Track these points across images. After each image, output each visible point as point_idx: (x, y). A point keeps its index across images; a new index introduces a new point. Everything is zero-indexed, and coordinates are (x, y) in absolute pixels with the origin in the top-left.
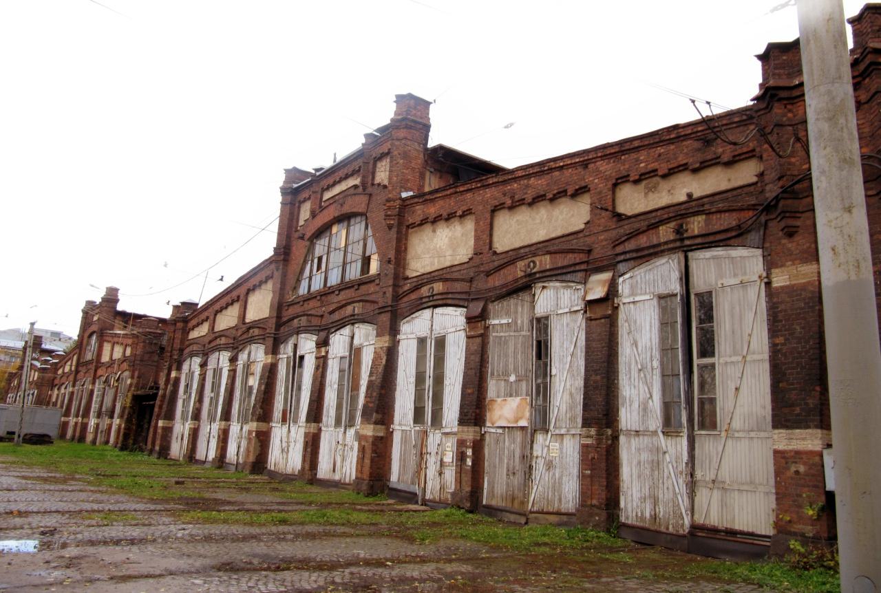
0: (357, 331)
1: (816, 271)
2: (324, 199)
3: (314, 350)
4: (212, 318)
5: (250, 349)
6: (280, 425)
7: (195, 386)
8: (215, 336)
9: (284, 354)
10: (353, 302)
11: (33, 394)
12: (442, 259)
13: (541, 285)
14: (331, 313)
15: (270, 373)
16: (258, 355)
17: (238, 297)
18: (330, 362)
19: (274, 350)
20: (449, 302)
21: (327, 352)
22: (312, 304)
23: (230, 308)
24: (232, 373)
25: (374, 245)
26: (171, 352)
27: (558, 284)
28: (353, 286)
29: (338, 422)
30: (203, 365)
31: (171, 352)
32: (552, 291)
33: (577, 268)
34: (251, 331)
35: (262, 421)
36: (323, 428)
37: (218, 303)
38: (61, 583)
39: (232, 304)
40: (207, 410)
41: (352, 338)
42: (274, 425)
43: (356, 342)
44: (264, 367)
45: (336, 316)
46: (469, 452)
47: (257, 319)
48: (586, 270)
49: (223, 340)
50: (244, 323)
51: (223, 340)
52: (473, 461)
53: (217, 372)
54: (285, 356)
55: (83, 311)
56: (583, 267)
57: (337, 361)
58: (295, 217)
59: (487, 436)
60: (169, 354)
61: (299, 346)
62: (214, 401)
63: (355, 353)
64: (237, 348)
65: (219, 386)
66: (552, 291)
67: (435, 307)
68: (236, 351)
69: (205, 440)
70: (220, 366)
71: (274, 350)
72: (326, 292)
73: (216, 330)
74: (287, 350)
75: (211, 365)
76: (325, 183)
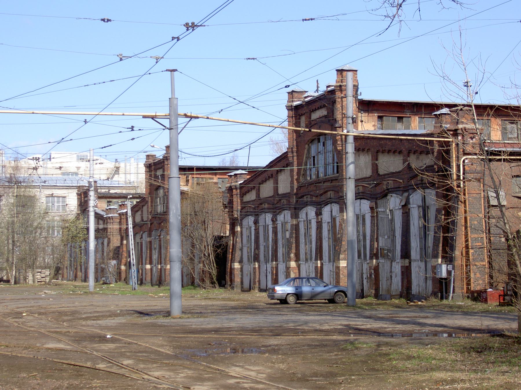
0: (333, 208)
1: (330, 210)
3: (315, 217)
5: (307, 210)
6: (304, 263)
9: (302, 218)
10: (329, 191)
12: (128, 176)
13: (390, 194)
15: (296, 228)
16: (285, 217)
17: (272, 175)
18: (323, 225)
19: (295, 216)
22: (312, 188)
23: (268, 182)
24: (275, 229)
28: (329, 181)
29: (330, 261)
30: (256, 222)
32: (159, 212)
36: (324, 264)
37: (260, 177)
38: (411, 335)
40: (247, 256)
41: (332, 212)
42: (301, 263)
43: (333, 214)
44: (292, 225)
47: (285, 192)
49: (266, 206)
50: (278, 195)
52: (375, 276)
53: (266, 227)
54: (302, 220)
55: (144, 165)
57: (326, 224)
59: (380, 264)
61: (308, 214)
62: (266, 247)
65: (268, 240)
66: (159, 212)
67: (361, 199)
69: (265, 275)
70: (267, 224)
71: (295, 216)
72: (318, 182)
74: (302, 215)
75: (261, 223)
76: (313, 107)
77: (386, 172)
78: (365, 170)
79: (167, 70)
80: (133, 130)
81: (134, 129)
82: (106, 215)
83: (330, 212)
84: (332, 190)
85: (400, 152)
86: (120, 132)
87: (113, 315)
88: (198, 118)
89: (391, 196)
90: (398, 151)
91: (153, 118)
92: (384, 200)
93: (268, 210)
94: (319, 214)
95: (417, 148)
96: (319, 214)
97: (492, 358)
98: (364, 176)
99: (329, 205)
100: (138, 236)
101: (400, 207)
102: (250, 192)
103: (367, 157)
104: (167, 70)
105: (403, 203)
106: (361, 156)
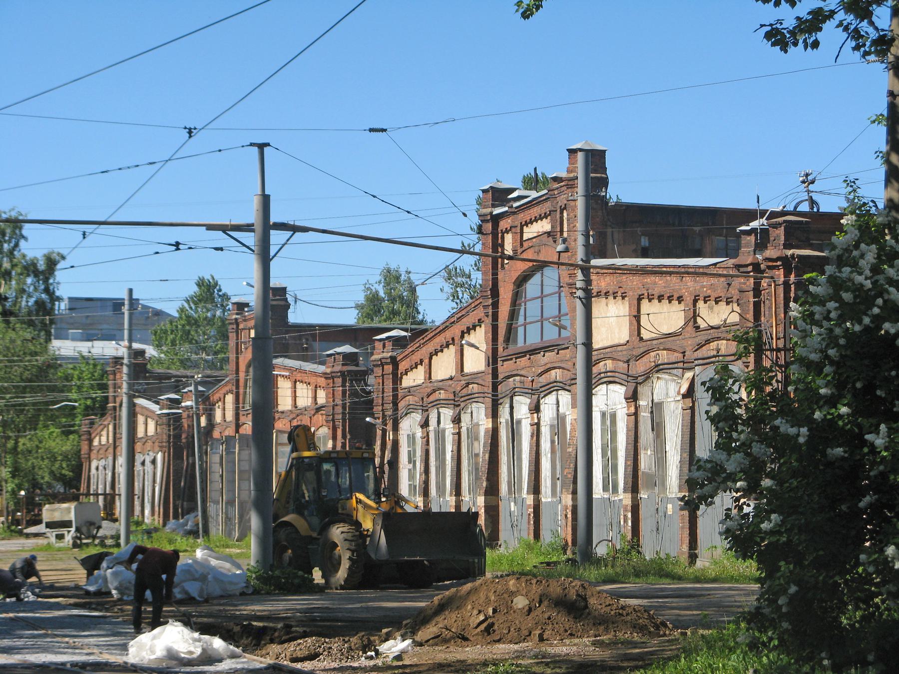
2: (525, 237)
4: (426, 361)
7: (419, 453)
8: (432, 387)
10: (554, 368)
11: (154, 462)
14: (541, 375)
17: (453, 339)
20: (617, 380)
21: (539, 419)
25: (263, 665)
26: (383, 405)
27: (666, 376)
31: (383, 405)
33: (676, 365)
34: (471, 386)
35: (491, 495)
39: (447, 346)
41: (558, 407)
43: (561, 410)
45: (543, 380)
46: (629, 515)
47: (475, 370)
48: (683, 369)
51: (442, 395)
56: (681, 365)
58: (558, 455)
60: (380, 408)
63: (560, 418)
64: (459, 405)
68: (458, 409)
73: (434, 378)
77: (654, 335)
78: (617, 331)
79: (252, 145)
80: (178, 249)
81: (181, 247)
82: (161, 409)
83: (555, 407)
84: (559, 368)
85: (680, 300)
86: (157, 253)
87: (341, 621)
88: (305, 230)
89: (658, 378)
90: (676, 296)
91: (224, 232)
92: (648, 384)
93: (445, 403)
94: (536, 409)
95: (709, 291)
96: (536, 409)
97: (469, 607)
98: (616, 342)
99: (554, 393)
100: (243, 453)
101: (680, 398)
102: (414, 370)
103: (621, 307)
104: (252, 145)
105: (684, 389)
106: (610, 306)
